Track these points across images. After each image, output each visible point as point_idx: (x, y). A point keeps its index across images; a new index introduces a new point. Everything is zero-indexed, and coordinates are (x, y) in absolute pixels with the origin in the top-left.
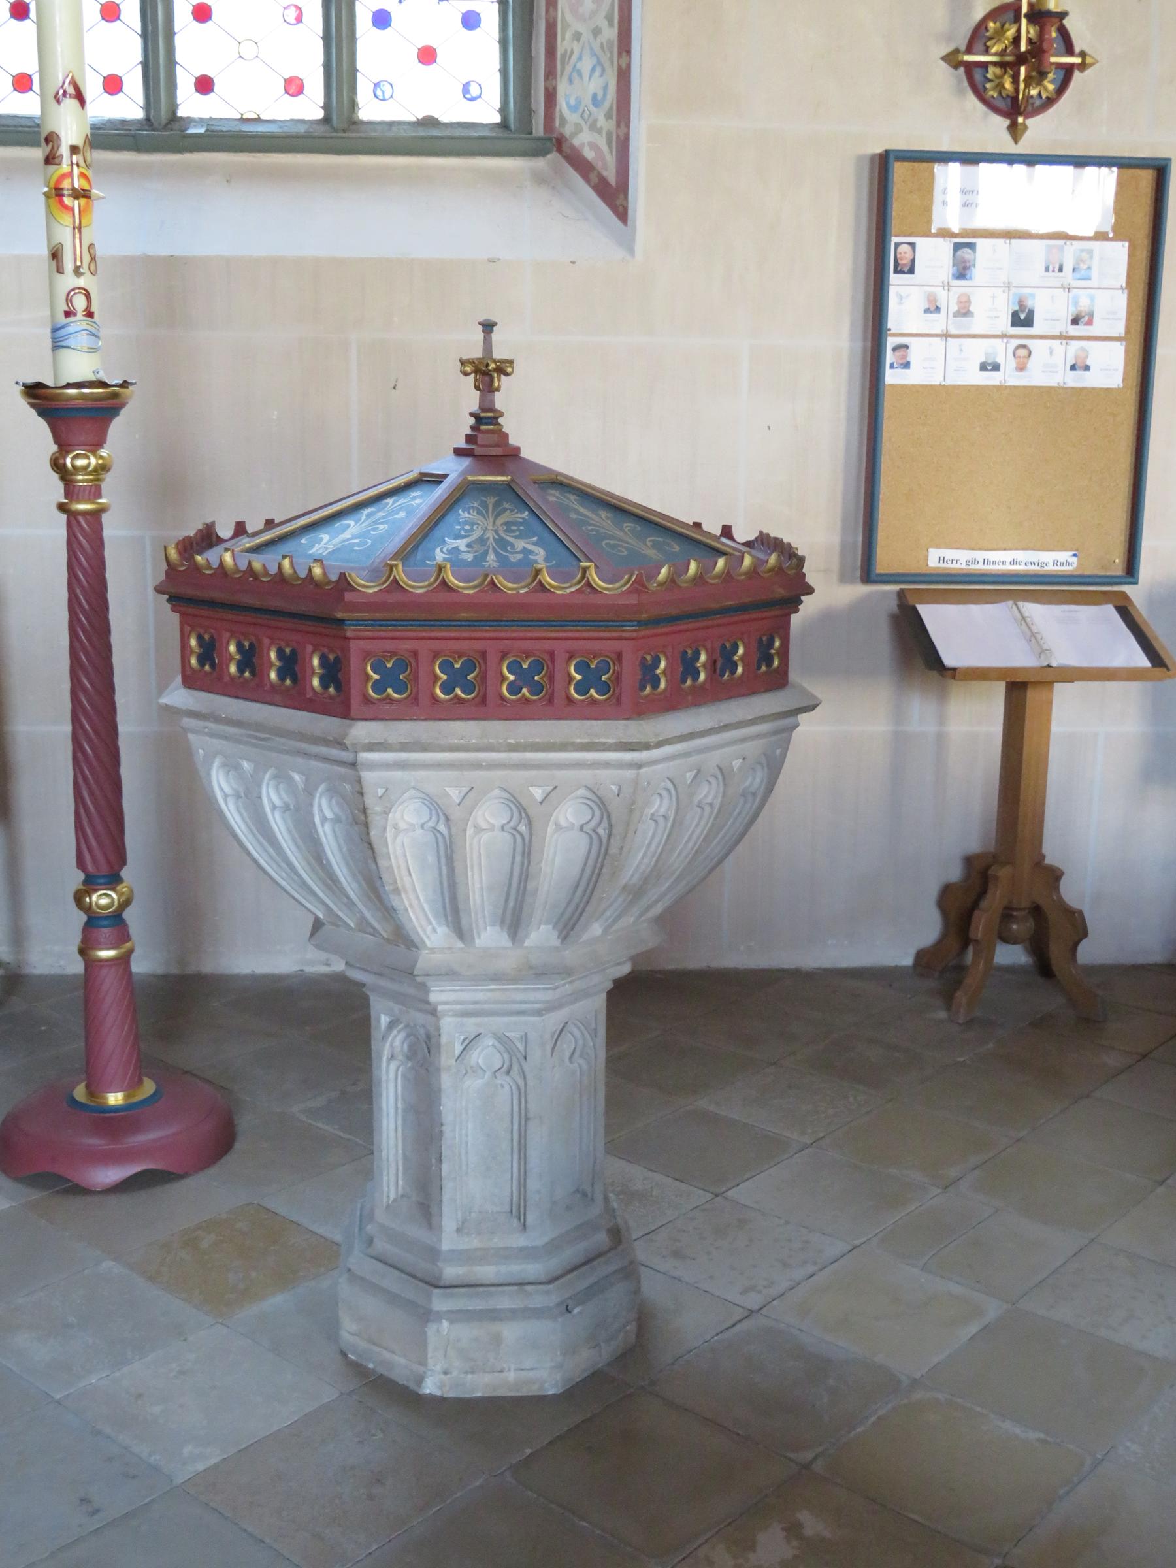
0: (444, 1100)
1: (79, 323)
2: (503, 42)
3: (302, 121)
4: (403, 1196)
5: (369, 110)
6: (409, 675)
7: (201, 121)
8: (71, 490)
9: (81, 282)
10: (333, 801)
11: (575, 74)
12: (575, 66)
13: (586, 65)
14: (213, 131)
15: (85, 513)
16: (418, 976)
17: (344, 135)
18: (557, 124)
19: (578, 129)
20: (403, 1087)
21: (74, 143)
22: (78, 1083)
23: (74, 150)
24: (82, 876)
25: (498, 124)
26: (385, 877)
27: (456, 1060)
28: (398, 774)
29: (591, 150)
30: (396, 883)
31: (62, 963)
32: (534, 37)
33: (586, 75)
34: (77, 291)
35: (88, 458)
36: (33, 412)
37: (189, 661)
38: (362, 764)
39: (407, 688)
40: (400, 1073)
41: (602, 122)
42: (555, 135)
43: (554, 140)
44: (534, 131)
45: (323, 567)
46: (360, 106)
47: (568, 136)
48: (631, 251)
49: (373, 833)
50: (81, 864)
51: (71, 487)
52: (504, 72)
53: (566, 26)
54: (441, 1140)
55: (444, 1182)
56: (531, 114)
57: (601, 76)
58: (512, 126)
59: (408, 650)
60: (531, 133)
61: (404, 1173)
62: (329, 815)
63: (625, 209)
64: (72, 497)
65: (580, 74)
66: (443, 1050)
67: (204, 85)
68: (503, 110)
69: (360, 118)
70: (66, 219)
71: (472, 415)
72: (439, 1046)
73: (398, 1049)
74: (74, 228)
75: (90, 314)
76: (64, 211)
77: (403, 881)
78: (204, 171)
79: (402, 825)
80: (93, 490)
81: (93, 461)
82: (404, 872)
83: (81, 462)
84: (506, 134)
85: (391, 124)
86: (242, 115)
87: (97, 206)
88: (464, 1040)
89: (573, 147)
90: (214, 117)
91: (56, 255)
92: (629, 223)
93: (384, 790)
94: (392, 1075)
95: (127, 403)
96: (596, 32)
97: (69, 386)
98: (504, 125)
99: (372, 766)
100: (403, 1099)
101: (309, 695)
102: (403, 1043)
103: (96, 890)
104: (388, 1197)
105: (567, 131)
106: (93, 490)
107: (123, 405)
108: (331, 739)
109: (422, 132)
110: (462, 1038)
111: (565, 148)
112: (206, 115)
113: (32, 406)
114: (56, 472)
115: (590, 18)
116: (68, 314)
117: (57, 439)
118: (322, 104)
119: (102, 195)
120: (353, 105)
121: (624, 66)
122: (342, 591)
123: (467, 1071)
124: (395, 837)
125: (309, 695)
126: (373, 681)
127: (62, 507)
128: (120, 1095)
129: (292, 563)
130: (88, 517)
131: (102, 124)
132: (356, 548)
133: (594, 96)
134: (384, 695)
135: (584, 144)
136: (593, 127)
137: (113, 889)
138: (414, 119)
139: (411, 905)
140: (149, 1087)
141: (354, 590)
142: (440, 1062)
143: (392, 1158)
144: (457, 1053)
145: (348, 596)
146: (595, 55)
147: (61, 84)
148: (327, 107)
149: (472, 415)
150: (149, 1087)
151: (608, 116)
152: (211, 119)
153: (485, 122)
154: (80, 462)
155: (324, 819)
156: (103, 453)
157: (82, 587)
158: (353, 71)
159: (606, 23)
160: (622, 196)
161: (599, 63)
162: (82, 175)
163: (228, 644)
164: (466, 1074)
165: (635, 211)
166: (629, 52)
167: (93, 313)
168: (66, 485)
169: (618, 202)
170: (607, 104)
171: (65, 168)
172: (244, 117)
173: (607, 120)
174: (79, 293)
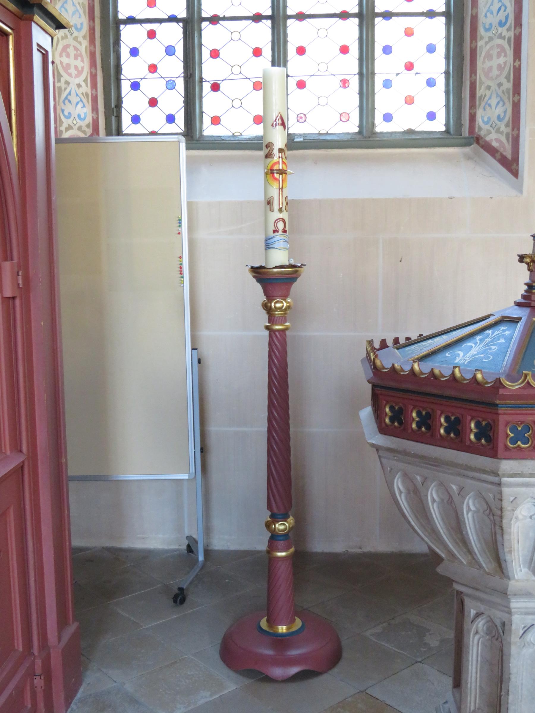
0: (512, 660)
1: (279, 236)
2: (447, 92)
3: (348, 133)
4: (479, 709)
5: (381, 127)
6: (531, 434)
7: (300, 135)
8: (272, 319)
9: (281, 216)
10: (476, 501)
11: (487, 106)
12: (487, 102)
13: (494, 101)
14: (306, 140)
15: (279, 331)
16: (510, 595)
17: (369, 139)
18: (477, 130)
19: (489, 132)
20: (482, 650)
21: (280, 147)
22: (263, 617)
23: (281, 150)
24: (269, 513)
25: (444, 131)
26: (506, 545)
27: (520, 638)
28: (523, 489)
29: (496, 142)
30: (511, 548)
31: (229, 544)
32: (463, 88)
33: (494, 107)
34: (279, 220)
35: (282, 303)
36: (254, 280)
37: (385, 421)
38: (505, 484)
39: (529, 443)
40: (480, 641)
41: (503, 128)
42: (475, 136)
43: (475, 138)
44: (463, 135)
45: (482, 373)
46: (376, 125)
47: (483, 136)
48: (521, 192)
49: (504, 521)
50: (269, 507)
51: (273, 318)
52: (447, 106)
53: (482, 83)
54: (509, 682)
55: (509, 705)
56: (461, 126)
57: (503, 106)
58: (452, 132)
59: (531, 421)
60: (461, 135)
61: (480, 696)
62: (473, 508)
63: (517, 171)
64: (273, 322)
65: (490, 106)
66: (513, 632)
67: (216, 121)
68: (447, 125)
69: (376, 131)
70: (275, 185)
71: (526, 284)
72: (510, 630)
73: (480, 629)
74: (279, 189)
75: (285, 231)
76: (275, 181)
77: (515, 546)
78: (304, 159)
79: (520, 517)
80: (283, 319)
81: (285, 304)
82: (516, 541)
83: (278, 304)
84: (449, 136)
85: (392, 133)
86: (319, 131)
87: (289, 177)
88: (524, 627)
89: (486, 142)
90: (305, 133)
91: (269, 202)
92: (519, 177)
93: (514, 498)
94: (476, 642)
95: (301, 275)
96: (500, 85)
97: (276, 267)
98: (447, 132)
99: (510, 485)
100: (481, 656)
101: (468, 443)
102: (484, 625)
103: (278, 522)
104: (470, 709)
105: (482, 133)
106: (283, 319)
107: (299, 276)
108: (489, 470)
109: (407, 137)
110: (523, 626)
111: (481, 142)
112: (302, 132)
113: (254, 277)
114: (265, 310)
115: (496, 78)
116: (274, 231)
117: (266, 293)
118: (358, 125)
119: (293, 172)
120: (373, 125)
121: (516, 101)
122: (498, 388)
123: (524, 644)
124: (516, 523)
125: (468, 443)
126: (510, 437)
127: (267, 328)
128: (284, 627)
129: (460, 370)
130: (281, 332)
131: (253, 138)
132: (484, 360)
133: (499, 117)
134: (516, 445)
135: (492, 140)
136: (498, 131)
137: (285, 521)
138: (402, 130)
139: (515, 559)
140: (298, 623)
141: (505, 387)
142: (510, 639)
143: (473, 687)
144: (520, 635)
145: (501, 391)
146: (499, 96)
147: (274, 120)
148: (360, 126)
149: (526, 284)
150: (298, 623)
151: (507, 125)
152: (304, 134)
153: (437, 131)
154: (278, 305)
155: (434, 501)
156: (289, 300)
157: (276, 367)
158: (374, 109)
159: (505, 80)
160: (515, 165)
161: (501, 99)
162: (283, 162)
163: (412, 412)
164: (523, 647)
165: (523, 171)
166: (519, 94)
167: (287, 230)
168: (269, 317)
169: (514, 166)
170: (507, 119)
171: (276, 159)
172: (320, 132)
173: (506, 127)
174: (280, 221)
